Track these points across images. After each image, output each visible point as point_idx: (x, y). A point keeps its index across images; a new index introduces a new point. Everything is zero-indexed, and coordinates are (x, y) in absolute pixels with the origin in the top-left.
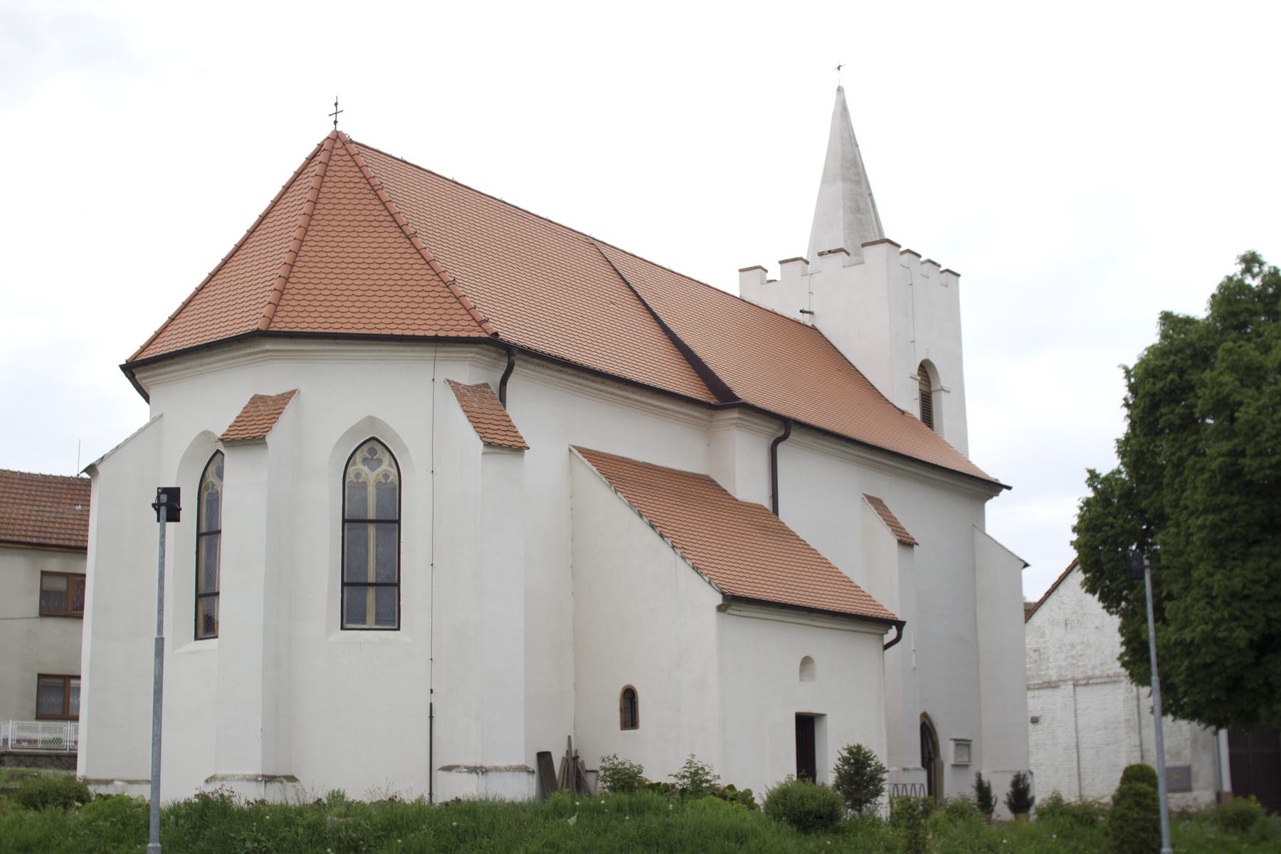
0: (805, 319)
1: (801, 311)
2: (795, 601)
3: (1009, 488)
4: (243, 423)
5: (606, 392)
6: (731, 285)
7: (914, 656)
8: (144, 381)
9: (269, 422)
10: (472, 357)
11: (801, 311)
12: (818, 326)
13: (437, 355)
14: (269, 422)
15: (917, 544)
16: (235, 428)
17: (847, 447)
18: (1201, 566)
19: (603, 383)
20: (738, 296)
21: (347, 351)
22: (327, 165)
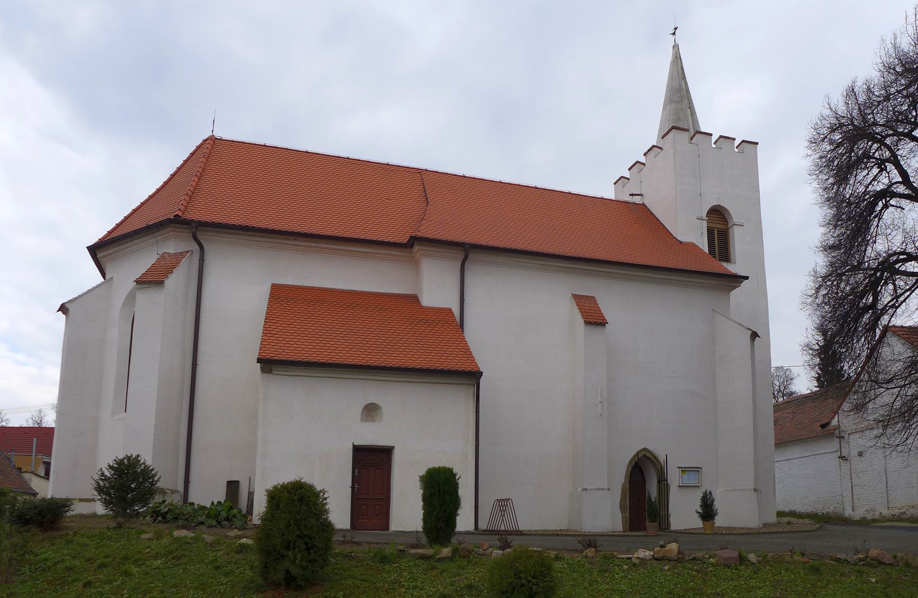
0: (637, 200)
1: (630, 195)
2: (349, 361)
3: (747, 278)
4: (164, 272)
5: (291, 245)
6: (609, 193)
7: (600, 406)
8: (102, 260)
9: (167, 272)
10: (173, 235)
11: (630, 195)
12: (646, 203)
13: (157, 239)
14: (167, 272)
15: (607, 323)
16: (145, 275)
17: (544, 260)
18: (8, 529)
19: (296, 239)
20: (613, 198)
21: (430, 251)
22: (199, 179)
